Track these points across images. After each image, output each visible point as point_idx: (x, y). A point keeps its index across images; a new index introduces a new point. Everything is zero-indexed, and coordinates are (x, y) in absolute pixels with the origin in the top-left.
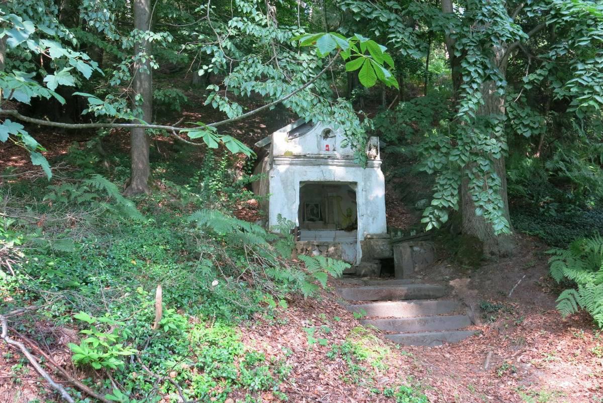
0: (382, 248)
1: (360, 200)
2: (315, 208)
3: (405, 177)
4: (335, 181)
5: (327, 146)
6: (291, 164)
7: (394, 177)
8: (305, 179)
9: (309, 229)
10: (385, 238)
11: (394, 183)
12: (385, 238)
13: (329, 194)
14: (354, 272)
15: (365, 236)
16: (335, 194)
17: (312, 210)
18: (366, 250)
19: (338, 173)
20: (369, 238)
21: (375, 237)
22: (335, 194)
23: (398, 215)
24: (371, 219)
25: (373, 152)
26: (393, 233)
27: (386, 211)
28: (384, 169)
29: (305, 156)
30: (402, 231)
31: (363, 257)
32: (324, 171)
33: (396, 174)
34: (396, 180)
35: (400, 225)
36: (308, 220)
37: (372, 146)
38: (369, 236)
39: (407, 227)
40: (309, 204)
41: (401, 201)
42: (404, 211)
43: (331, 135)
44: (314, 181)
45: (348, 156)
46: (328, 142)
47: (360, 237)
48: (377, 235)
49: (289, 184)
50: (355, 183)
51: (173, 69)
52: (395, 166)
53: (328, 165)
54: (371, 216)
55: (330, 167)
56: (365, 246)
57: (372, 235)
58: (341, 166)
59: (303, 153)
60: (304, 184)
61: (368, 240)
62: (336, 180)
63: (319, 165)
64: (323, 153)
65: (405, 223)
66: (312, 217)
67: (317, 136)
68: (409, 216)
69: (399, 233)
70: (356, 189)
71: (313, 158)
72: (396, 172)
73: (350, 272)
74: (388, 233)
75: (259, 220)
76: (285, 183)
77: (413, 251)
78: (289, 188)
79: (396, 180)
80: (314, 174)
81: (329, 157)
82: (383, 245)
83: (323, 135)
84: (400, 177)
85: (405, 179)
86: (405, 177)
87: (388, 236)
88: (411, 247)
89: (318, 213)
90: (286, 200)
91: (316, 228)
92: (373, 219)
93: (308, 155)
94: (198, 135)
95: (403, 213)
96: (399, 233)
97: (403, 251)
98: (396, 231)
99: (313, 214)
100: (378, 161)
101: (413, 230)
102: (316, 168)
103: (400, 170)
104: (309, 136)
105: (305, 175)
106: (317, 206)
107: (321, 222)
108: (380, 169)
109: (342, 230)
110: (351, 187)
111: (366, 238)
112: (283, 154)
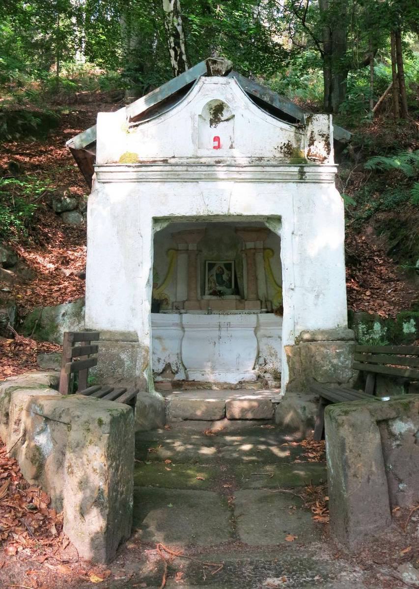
0: (335, 361)
1: (288, 255)
3: (398, 209)
5: (217, 139)
6: (139, 180)
7: (377, 210)
9: (210, 312)
10: (342, 339)
11: (377, 221)
12: (342, 339)
13: (250, 245)
14: (270, 416)
15: (297, 334)
16: (260, 245)
17: (219, 275)
18: (297, 366)
19: (237, 198)
20: (308, 341)
21: (320, 337)
22: (260, 245)
23: (377, 283)
24: (311, 297)
25: (319, 148)
26: (362, 327)
28: (343, 183)
29: (165, 161)
30: (383, 322)
31: (290, 382)
33: (381, 204)
34: (381, 216)
35: (381, 306)
36: (210, 294)
37: (316, 137)
38: (306, 336)
39: (395, 312)
40: (214, 264)
41: (389, 254)
42: (391, 275)
43: (226, 115)
45: (260, 159)
46: (221, 129)
48: (323, 332)
50: (278, 219)
51: (117, 96)
52: (381, 191)
53: (214, 179)
55: (221, 185)
56: (296, 358)
57: (314, 333)
58: (244, 180)
59: (160, 156)
60: (165, 225)
61: (304, 346)
63: (196, 180)
64: (208, 153)
65: (391, 303)
66: (219, 288)
67: (192, 118)
68: (401, 285)
69: (377, 326)
71: (181, 165)
72: (381, 201)
73: (261, 416)
74: (350, 326)
75: (70, 302)
77: (392, 435)
79: (381, 216)
80: (188, 202)
81: (219, 162)
82: (338, 355)
83: (209, 117)
84: (389, 211)
85: (398, 213)
86: (398, 209)
87: (351, 333)
88: (383, 423)
89: (230, 278)
91: (223, 311)
92: (317, 296)
93: (172, 161)
95: (390, 280)
96: (377, 326)
97: (349, 440)
98: (369, 321)
99: (221, 282)
100: (329, 168)
101: (408, 319)
103: (390, 199)
106: (228, 267)
107: (234, 297)
108: (334, 185)
109: (272, 312)
110: (270, 226)
111: (298, 340)
112: (117, 159)
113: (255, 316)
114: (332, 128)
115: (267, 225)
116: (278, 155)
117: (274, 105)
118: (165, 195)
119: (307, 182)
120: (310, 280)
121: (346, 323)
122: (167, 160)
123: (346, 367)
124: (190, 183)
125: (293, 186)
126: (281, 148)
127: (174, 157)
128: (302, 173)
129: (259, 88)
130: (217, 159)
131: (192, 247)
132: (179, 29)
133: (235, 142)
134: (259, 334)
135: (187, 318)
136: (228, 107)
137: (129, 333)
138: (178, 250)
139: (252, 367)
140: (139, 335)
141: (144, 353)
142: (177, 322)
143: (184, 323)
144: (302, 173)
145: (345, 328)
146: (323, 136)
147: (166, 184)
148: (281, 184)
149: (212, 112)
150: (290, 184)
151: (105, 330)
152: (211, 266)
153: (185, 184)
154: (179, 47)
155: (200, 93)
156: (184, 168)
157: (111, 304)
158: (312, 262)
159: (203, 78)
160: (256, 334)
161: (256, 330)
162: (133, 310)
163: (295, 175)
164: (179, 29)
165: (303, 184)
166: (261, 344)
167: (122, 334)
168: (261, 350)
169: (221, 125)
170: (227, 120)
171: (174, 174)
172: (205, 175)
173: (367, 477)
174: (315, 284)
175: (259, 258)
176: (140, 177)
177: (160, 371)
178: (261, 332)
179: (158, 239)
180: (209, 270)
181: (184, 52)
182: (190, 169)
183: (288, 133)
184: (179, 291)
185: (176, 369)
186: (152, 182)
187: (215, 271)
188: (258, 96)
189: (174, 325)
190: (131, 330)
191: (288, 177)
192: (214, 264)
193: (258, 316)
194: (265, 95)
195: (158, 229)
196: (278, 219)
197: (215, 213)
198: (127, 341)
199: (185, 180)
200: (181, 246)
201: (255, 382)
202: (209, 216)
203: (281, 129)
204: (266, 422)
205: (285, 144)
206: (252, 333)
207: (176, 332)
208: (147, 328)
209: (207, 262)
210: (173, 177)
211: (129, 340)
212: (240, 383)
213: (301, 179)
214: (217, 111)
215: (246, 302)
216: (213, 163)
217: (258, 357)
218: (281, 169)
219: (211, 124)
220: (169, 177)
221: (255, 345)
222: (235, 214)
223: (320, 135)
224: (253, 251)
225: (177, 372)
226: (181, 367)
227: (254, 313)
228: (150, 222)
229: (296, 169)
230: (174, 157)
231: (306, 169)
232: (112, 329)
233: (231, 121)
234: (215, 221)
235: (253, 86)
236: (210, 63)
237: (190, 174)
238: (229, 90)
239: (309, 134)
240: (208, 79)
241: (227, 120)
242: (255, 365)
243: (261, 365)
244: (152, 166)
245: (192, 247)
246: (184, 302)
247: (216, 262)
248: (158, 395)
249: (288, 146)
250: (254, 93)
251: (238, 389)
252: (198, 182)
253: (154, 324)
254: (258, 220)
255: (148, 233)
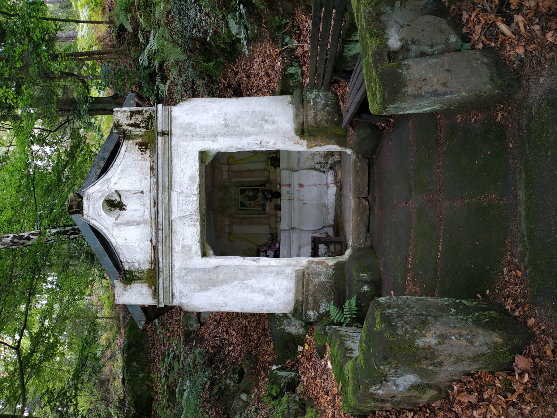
2: (247, 193)
4: (200, 193)
8: (196, 247)
13: (225, 176)
16: (225, 168)
17: (250, 198)
22: (225, 168)
24: (267, 126)
27: (220, 96)
32: (181, 214)
37: (132, 121)
40: (241, 202)
43: (116, 198)
44: (201, 232)
47: (300, 146)
48: (297, 116)
49: (207, 277)
50: (203, 154)
54: (261, 125)
60: (208, 247)
61: (303, 131)
62: (197, 192)
63: (170, 223)
70: (213, 152)
74: (291, 94)
76: (208, 282)
78: (213, 276)
90: (236, 282)
92: (266, 121)
93: (154, 241)
94: (229, 129)
102: (178, 227)
104: (119, 240)
105: (190, 249)
106: (243, 191)
108: (174, 108)
110: (209, 160)
113: (282, 171)
114: (125, 109)
115: (207, 163)
116: (148, 153)
117: (107, 157)
118: (183, 247)
119: (171, 130)
120: (252, 127)
121: (288, 96)
122: (154, 247)
123: (326, 96)
124: (173, 227)
125: (174, 140)
126: (142, 151)
127: (151, 241)
128: (163, 134)
129: (94, 170)
130: (152, 205)
131: (227, 221)
132: (54, 231)
133: (138, 189)
134: (296, 169)
135: (284, 225)
136: (108, 196)
137: (297, 277)
138: (230, 233)
139: (323, 174)
140: (298, 268)
141: (313, 265)
142: (287, 234)
143: (287, 228)
144: (163, 134)
145: (293, 98)
146: (131, 116)
147: (174, 247)
148: (173, 151)
149: (113, 209)
150: (172, 144)
151: (294, 297)
152: (243, 205)
153: (173, 231)
154: (68, 231)
155: (97, 219)
156: (160, 232)
157: (274, 291)
158: (238, 126)
159: (84, 217)
160: (297, 171)
161: (293, 171)
162: (277, 273)
163: (165, 140)
164: (54, 231)
165: (172, 132)
166: (304, 167)
167: (297, 282)
168: (309, 167)
169: (124, 201)
170: (120, 196)
171: (166, 240)
172: (165, 215)
173: (446, 73)
174: (255, 123)
175: (235, 168)
176: (168, 268)
177: (326, 247)
178: (295, 166)
179: (221, 252)
180: (246, 207)
181: (72, 227)
182: (160, 227)
183: (129, 146)
184: (261, 231)
185: (324, 235)
186: (172, 258)
187: (246, 202)
188: (100, 170)
189: (289, 236)
190: (294, 275)
191: (167, 146)
192: (241, 202)
193: (282, 169)
194: (99, 165)
195: (212, 252)
196: (203, 154)
197: (198, 206)
198: (304, 279)
199: (171, 231)
200: (227, 230)
201: (335, 172)
202: (200, 212)
203: (126, 151)
204: (371, 165)
205: (139, 148)
206: (296, 173)
207: (295, 235)
208: (293, 260)
209: (240, 208)
210: (168, 241)
211: (303, 278)
212: (336, 183)
213: (168, 134)
214: (114, 205)
215: (271, 178)
216: (156, 209)
217: (315, 169)
218: (160, 152)
219: (124, 209)
220: (167, 245)
221: (306, 171)
222: (198, 190)
223: (131, 119)
224: (230, 173)
225: (327, 234)
226: (323, 230)
227: (280, 172)
228: (206, 259)
229: (160, 138)
230: (151, 241)
231: (160, 130)
232: (293, 291)
233: (120, 193)
234: (204, 206)
235: (91, 174)
236: (71, 211)
237: (165, 227)
238: (95, 194)
239: (130, 128)
240: (85, 211)
241: (120, 196)
242: (321, 171)
243: (321, 167)
244: (158, 259)
245: (227, 221)
246: (271, 228)
247: (240, 204)
248: (348, 252)
249: (140, 145)
250: (98, 173)
251: (341, 185)
252: (172, 221)
253: (289, 256)
254: (203, 171)
255: (214, 261)
